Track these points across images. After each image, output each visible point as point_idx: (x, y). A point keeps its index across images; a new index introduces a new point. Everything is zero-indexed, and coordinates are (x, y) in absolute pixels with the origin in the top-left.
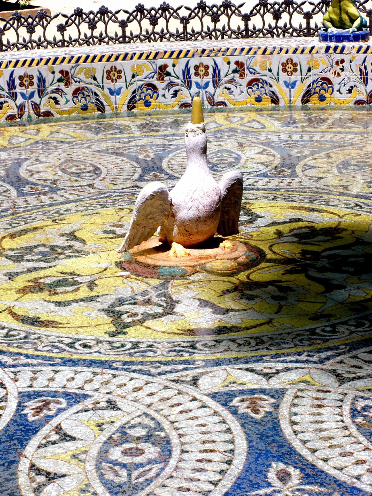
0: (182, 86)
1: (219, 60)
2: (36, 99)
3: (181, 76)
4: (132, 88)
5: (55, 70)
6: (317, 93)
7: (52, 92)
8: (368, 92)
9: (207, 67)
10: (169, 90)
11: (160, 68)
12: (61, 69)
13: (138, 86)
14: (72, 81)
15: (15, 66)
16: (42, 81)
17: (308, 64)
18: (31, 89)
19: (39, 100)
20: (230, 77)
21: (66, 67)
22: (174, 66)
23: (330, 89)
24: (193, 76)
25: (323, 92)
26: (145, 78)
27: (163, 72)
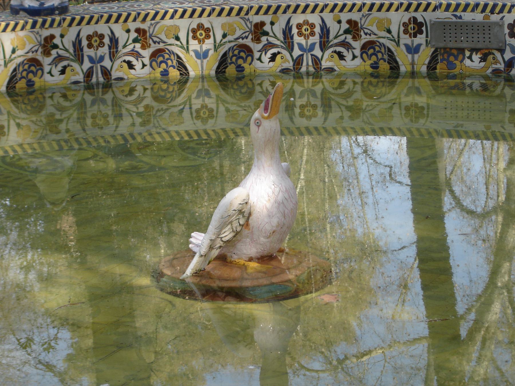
0: (72, 60)
1: (118, 30)
2: (317, 52)
3: (71, 50)
4: (222, 51)
5: (342, 19)
6: (23, 77)
7: (337, 45)
8: (85, 71)
9: (102, 37)
10: (56, 66)
11: (256, 25)
12: (349, 18)
13: (229, 47)
14: (151, 42)
15: (295, 11)
16: (114, 41)
17: (12, 44)
18: (312, 40)
19: (321, 53)
20: (342, 38)
21: (355, 16)
22: (62, 36)
23: (40, 72)
24: (86, 49)
25: (31, 76)
26: (28, 53)
27: (259, 31)
